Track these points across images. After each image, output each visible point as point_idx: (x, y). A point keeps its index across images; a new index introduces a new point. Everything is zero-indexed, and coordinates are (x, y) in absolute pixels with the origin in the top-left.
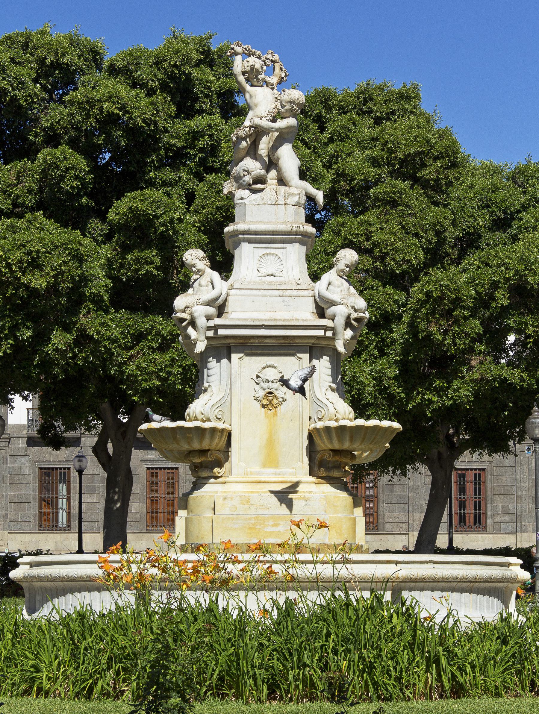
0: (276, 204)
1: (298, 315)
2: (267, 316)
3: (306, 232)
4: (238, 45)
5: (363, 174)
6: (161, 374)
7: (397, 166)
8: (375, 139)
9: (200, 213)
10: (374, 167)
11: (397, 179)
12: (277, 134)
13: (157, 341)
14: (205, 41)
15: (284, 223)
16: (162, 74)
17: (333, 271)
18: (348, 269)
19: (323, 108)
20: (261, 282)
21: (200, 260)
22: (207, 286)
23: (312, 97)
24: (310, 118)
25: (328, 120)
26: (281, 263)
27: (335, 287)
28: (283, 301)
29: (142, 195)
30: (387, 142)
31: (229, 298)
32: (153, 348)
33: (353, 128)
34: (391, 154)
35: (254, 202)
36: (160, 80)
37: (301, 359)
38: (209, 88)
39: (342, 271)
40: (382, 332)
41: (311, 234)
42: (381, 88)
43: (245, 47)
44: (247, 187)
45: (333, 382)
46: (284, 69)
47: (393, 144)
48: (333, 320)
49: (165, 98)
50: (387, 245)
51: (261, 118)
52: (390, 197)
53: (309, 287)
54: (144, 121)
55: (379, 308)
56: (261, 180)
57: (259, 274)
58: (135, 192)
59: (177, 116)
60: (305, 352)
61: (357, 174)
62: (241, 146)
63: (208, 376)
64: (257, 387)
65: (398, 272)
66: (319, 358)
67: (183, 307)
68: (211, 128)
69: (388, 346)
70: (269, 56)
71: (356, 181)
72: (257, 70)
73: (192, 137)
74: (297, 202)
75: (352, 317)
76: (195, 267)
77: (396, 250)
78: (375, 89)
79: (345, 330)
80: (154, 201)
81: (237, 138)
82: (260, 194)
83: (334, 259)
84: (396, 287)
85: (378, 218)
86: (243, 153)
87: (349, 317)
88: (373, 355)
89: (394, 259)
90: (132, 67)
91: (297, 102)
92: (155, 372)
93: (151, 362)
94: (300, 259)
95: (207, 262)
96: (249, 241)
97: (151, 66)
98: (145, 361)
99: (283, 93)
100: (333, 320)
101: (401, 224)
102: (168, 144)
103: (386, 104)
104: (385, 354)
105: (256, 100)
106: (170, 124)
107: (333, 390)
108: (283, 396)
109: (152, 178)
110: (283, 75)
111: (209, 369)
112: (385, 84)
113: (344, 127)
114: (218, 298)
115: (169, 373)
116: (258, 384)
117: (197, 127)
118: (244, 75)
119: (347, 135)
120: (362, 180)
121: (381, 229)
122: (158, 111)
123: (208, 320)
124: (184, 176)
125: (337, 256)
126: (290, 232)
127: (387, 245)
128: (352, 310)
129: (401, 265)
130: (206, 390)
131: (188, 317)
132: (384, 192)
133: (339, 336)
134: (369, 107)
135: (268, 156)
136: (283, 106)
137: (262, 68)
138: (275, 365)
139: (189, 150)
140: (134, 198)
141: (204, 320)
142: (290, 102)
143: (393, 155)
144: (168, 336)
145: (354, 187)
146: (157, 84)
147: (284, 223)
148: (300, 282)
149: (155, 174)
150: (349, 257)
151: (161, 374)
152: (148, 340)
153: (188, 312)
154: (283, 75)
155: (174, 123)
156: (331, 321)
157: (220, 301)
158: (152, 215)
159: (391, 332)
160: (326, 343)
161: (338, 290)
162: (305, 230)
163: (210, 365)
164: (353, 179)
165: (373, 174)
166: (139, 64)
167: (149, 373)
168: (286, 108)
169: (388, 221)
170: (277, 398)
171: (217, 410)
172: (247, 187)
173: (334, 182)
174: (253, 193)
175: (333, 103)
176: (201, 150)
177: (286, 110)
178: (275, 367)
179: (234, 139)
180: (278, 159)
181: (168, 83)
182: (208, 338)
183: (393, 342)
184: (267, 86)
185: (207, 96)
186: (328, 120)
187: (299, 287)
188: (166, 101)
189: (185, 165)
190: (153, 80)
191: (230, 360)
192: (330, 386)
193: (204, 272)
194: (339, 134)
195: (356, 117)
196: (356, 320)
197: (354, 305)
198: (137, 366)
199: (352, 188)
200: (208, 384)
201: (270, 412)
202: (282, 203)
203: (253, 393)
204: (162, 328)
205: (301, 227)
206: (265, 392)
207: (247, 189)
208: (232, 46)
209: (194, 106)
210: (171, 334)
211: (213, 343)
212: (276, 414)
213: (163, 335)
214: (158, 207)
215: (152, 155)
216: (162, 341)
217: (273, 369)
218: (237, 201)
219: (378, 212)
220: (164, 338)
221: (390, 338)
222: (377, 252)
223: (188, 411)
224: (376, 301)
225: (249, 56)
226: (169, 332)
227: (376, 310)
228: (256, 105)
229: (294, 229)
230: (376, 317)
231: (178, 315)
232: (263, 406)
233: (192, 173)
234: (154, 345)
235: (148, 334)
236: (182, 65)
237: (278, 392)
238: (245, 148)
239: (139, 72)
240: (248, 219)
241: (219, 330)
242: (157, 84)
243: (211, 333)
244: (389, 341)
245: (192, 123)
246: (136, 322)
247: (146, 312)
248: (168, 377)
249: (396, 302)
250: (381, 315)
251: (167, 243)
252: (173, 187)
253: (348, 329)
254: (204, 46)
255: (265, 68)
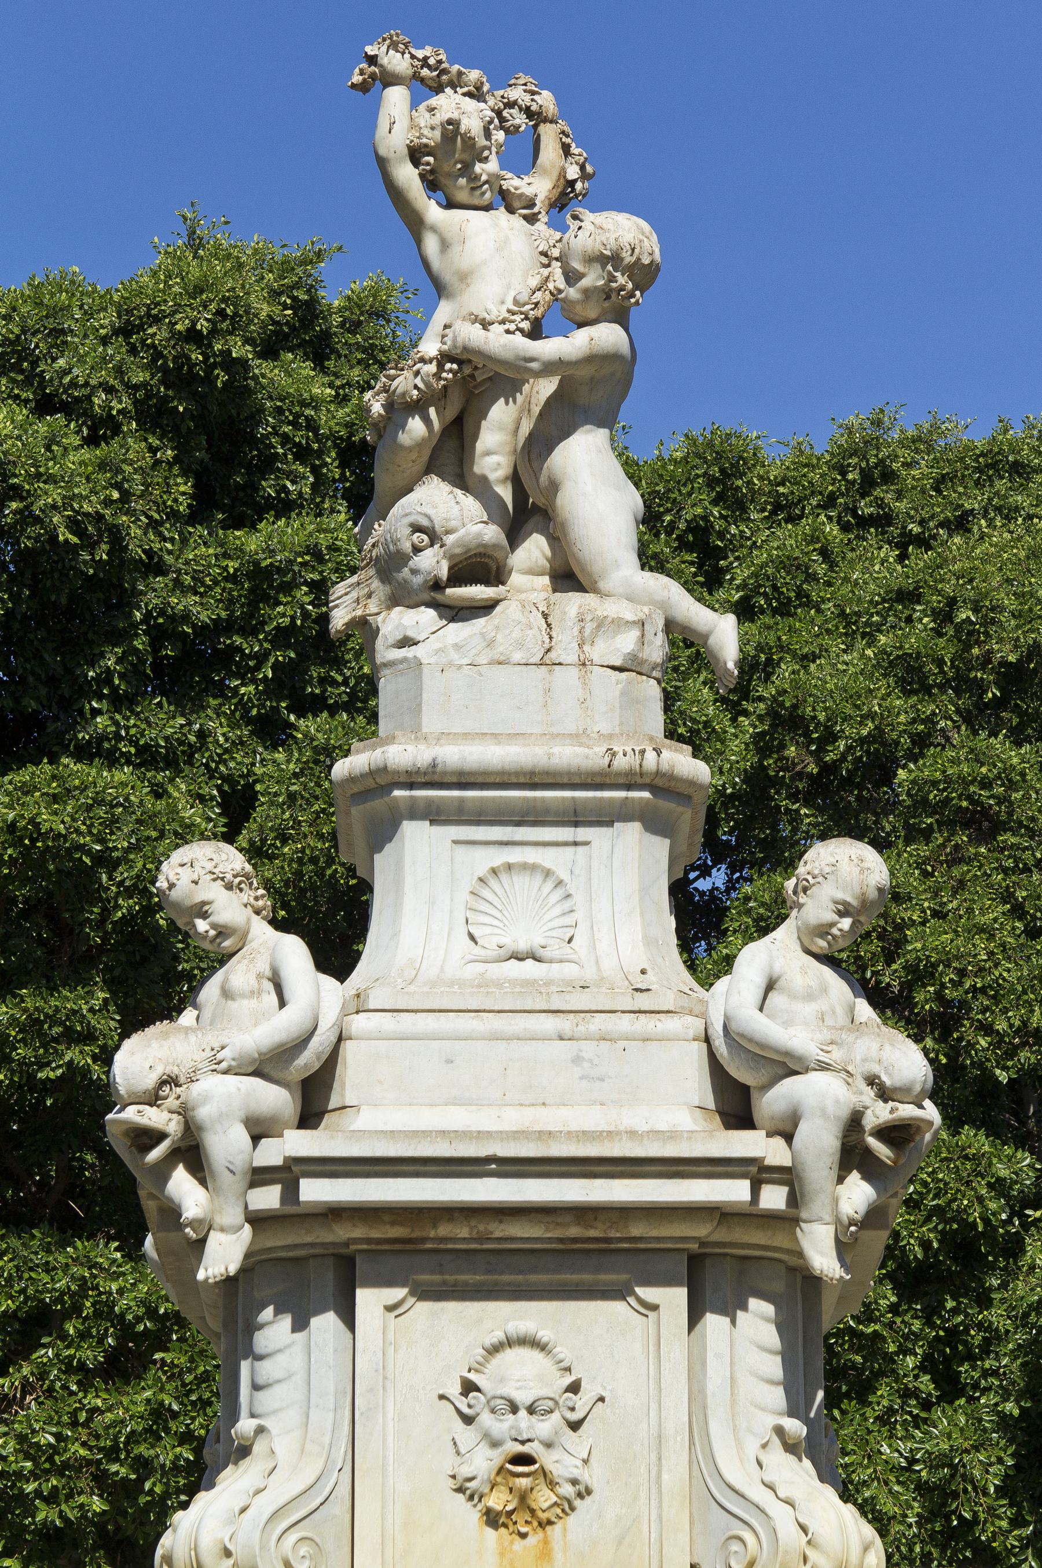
0: (547, 662)
1: (636, 1119)
2: (512, 1119)
3: (671, 777)
4: (394, 46)
5: (871, 715)
6: (114, 1468)
7: (993, 692)
8: (907, 597)
9: (271, 858)
10: (907, 693)
11: (994, 734)
12: (546, 387)
13: (101, 1341)
14: (299, 270)
15: (577, 738)
16: (144, 368)
17: (784, 935)
18: (846, 923)
19: (715, 502)
20: (483, 984)
21: (229, 887)
22: (255, 994)
23: (676, 462)
24: (669, 534)
25: (732, 546)
26: (567, 905)
27: (793, 996)
28: (577, 1060)
29: (54, 777)
30: (952, 602)
31: (349, 1049)
32: (82, 1366)
33: (821, 569)
34: (968, 648)
35: (454, 656)
36: (136, 387)
37: (654, 1308)
38: (312, 425)
39: (823, 930)
40: (950, 1304)
41: (692, 783)
42: (920, 442)
43: (420, 54)
44: (426, 596)
45: (792, 1412)
46: (575, 150)
47: (976, 610)
48: (789, 1138)
49: (153, 450)
50: (962, 973)
51: (485, 325)
52: (969, 798)
53: (685, 1002)
54: (75, 525)
55: (937, 1210)
56: (486, 567)
57: (477, 951)
58: (31, 768)
59: (195, 517)
60: (668, 1281)
61: (846, 718)
62: (404, 438)
63: (256, 1387)
64: (466, 1436)
65: (1003, 1076)
66: (731, 1307)
67: (150, 1081)
68: (318, 557)
69: (970, 1357)
70: (516, 94)
71: (842, 745)
72: (469, 142)
73: (251, 591)
74: (633, 657)
75: (870, 1122)
76: (205, 916)
77: (996, 993)
78: (901, 442)
79: (841, 1180)
80: (98, 801)
81: (389, 406)
82: (480, 623)
83: (790, 884)
84: (995, 1131)
85: (926, 874)
86: (411, 465)
87: (854, 1122)
88: (915, 1393)
89: (987, 1029)
90: (37, 344)
91: (628, 259)
92: (89, 1463)
93: (74, 1424)
94: (644, 890)
95: (256, 895)
96: (436, 815)
97: (105, 341)
98: (49, 1421)
99: (573, 225)
100: (789, 1138)
101: (1007, 896)
102: (162, 613)
103: (939, 491)
104: (960, 1392)
105: (464, 257)
106: (172, 540)
107: (791, 1447)
108: (576, 1473)
109: (103, 737)
110: (573, 172)
111: (260, 1358)
112: (935, 428)
113: (789, 564)
114: (303, 1042)
115: (144, 1466)
116: (468, 1420)
117: (272, 553)
118: (416, 163)
119: (800, 593)
120: (862, 741)
121: (936, 914)
122: (126, 496)
123: (256, 1139)
124: (220, 731)
125: (801, 870)
126: (601, 773)
127: (962, 973)
128: (870, 1093)
129: (1012, 1052)
130: (244, 1451)
131: (173, 1126)
132: (948, 780)
133: (817, 1207)
134: (880, 503)
135: (515, 479)
136: (571, 277)
137: (488, 134)
138: (544, 1335)
139: (238, 640)
140: (27, 789)
141: (240, 1136)
142: (602, 260)
143: (976, 651)
144: (139, 1319)
145: (835, 766)
146: (126, 402)
147: (577, 738)
148: (651, 980)
149: (116, 723)
150: (848, 871)
151: (114, 1468)
152: (63, 1336)
153: (171, 1102)
154: (573, 172)
155: (184, 541)
156: (779, 1142)
157: (309, 1059)
158: (89, 853)
159: (984, 1301)
160: (757, 1237)
161: (809, 1010)
162: (665, 767)
163: (263, 1340)
164: (830, 737)
165: (902, 718)
166: (63, 332)
167: (66, 1465)
168: (585, 282)
169: (962, 884)
170: (552, 1484)
171: (293, 1537)
172: (426, 596)
173: (763, 745)
174: (452, 620)
175: (750, 483)
176: (283, 637)
177: (587, 292)
178: (542, 1347)
179: (377, 408)
180: (554, 487)
181: (165, 399)
182: (257, 1220)
183: (993, 1338)
184: (511, 210)
185: (302, 454)
186: (732, 546)
187: (644, 1002)
188: (157, 463)
189: (221, 691)
190: (110, 390)
191: (349, 1319)
192: (779, 1431)
193: (243, 937)
194: (775, 588)
195: (832, 530)
196: (886, 1134)
197: (876, 1069)
198: (21, 1438)
199: (828, 769)
200: (254, 1423)
201: (519, 1544)
202: (572, 658)
203: (449, 1463)
204: (121, 1291)
205: (650, 756)
206: (498, 1456)
207: (429, 604)
208: (370, 50)
209: (255, 488)
210: (151, 1313)
211: (278, 1239)
212: (545, 1552)
213: (122, 1315)
214: (113, 823)
215: (102, 655)
216: (121, 1339)
217: (535, 1354)
218: (385, 652)
219: (924, 851)
220: (125, 1330)
221: (980, 1326)
222: (924, 997)
223: (166, 1541)
224: (925, 1184)
225: (439, 89)
226: (143, 1303)
227: (928, 1220)
228: (464, 277)
229: (621, 763)
230: (925, 1245)
231: (131, 1114)
232: (492, 1519)
233: (249, 721)
234: (90, 1355)
235: (66, 1315)
236: (214, 332)
237: (556, 1454)
238: (420, 444)
239: (61, 362)
240: (430, 722)
241: (304, 1183)
242: (126, 402)
243: (268, 1198)
244: (976, 1338)
245: (252, 542)
246: (25, 1266)
247: (62, 1230)
248: (141, 1481)
249: (999, 1187)
250: (944, 1237)
251: (144, 960)
252: (178, 772)
253: (855, 1177)
254: (296, 286)
255: (500, 136)
